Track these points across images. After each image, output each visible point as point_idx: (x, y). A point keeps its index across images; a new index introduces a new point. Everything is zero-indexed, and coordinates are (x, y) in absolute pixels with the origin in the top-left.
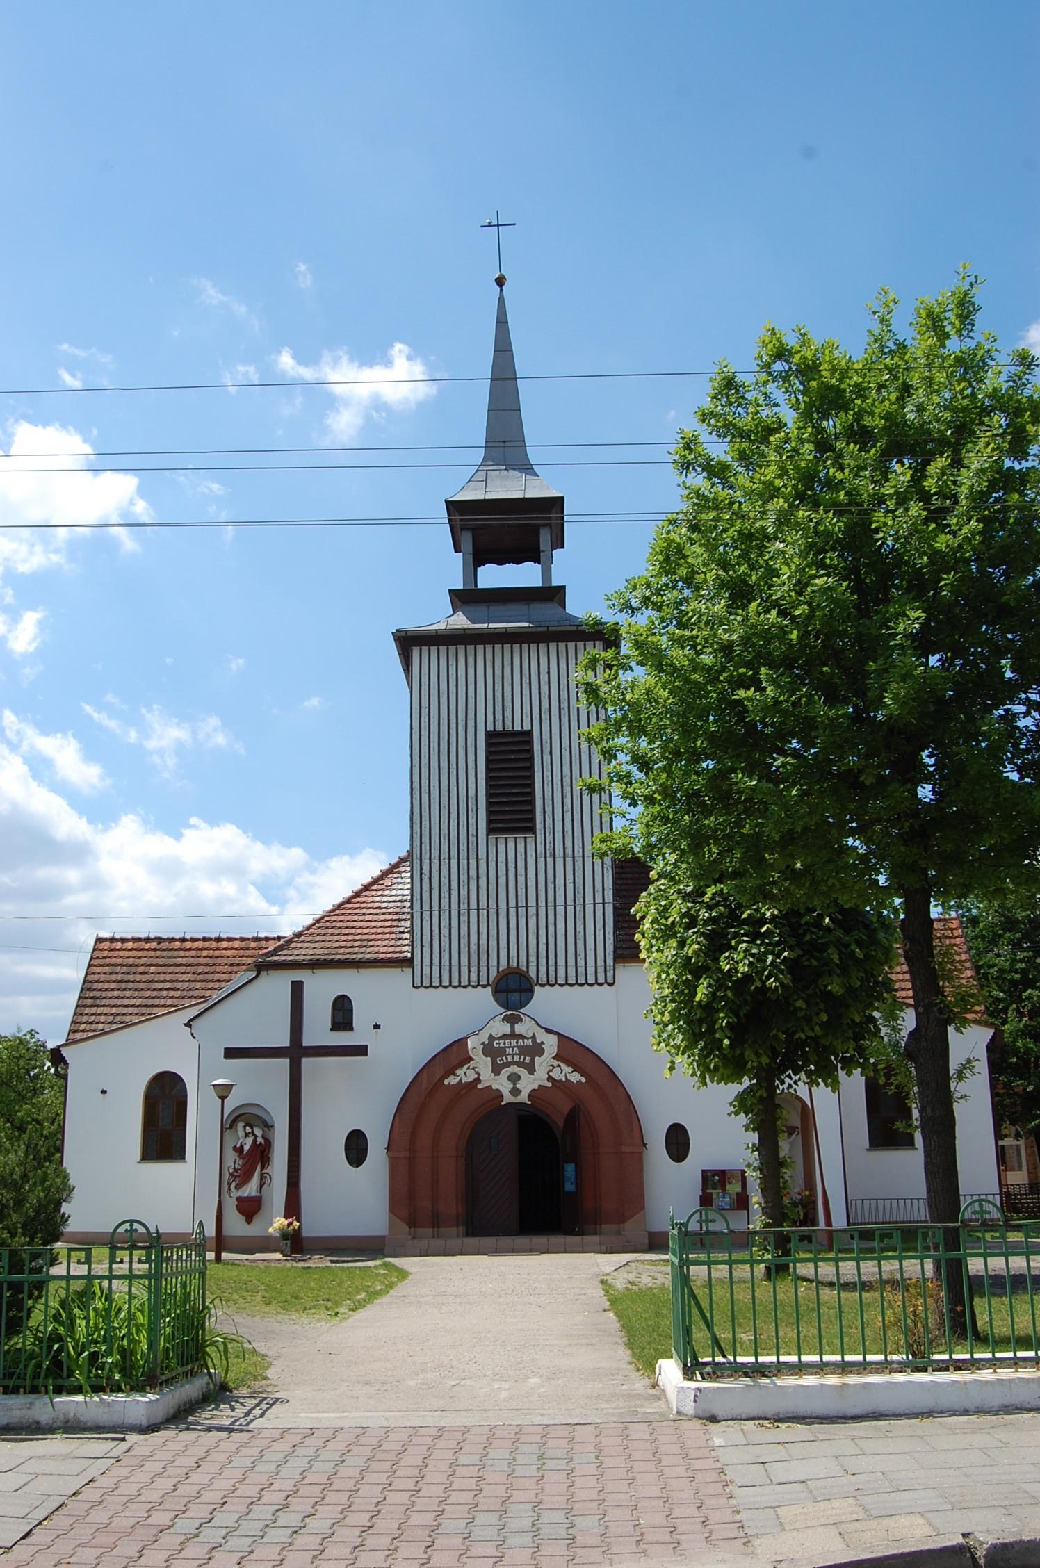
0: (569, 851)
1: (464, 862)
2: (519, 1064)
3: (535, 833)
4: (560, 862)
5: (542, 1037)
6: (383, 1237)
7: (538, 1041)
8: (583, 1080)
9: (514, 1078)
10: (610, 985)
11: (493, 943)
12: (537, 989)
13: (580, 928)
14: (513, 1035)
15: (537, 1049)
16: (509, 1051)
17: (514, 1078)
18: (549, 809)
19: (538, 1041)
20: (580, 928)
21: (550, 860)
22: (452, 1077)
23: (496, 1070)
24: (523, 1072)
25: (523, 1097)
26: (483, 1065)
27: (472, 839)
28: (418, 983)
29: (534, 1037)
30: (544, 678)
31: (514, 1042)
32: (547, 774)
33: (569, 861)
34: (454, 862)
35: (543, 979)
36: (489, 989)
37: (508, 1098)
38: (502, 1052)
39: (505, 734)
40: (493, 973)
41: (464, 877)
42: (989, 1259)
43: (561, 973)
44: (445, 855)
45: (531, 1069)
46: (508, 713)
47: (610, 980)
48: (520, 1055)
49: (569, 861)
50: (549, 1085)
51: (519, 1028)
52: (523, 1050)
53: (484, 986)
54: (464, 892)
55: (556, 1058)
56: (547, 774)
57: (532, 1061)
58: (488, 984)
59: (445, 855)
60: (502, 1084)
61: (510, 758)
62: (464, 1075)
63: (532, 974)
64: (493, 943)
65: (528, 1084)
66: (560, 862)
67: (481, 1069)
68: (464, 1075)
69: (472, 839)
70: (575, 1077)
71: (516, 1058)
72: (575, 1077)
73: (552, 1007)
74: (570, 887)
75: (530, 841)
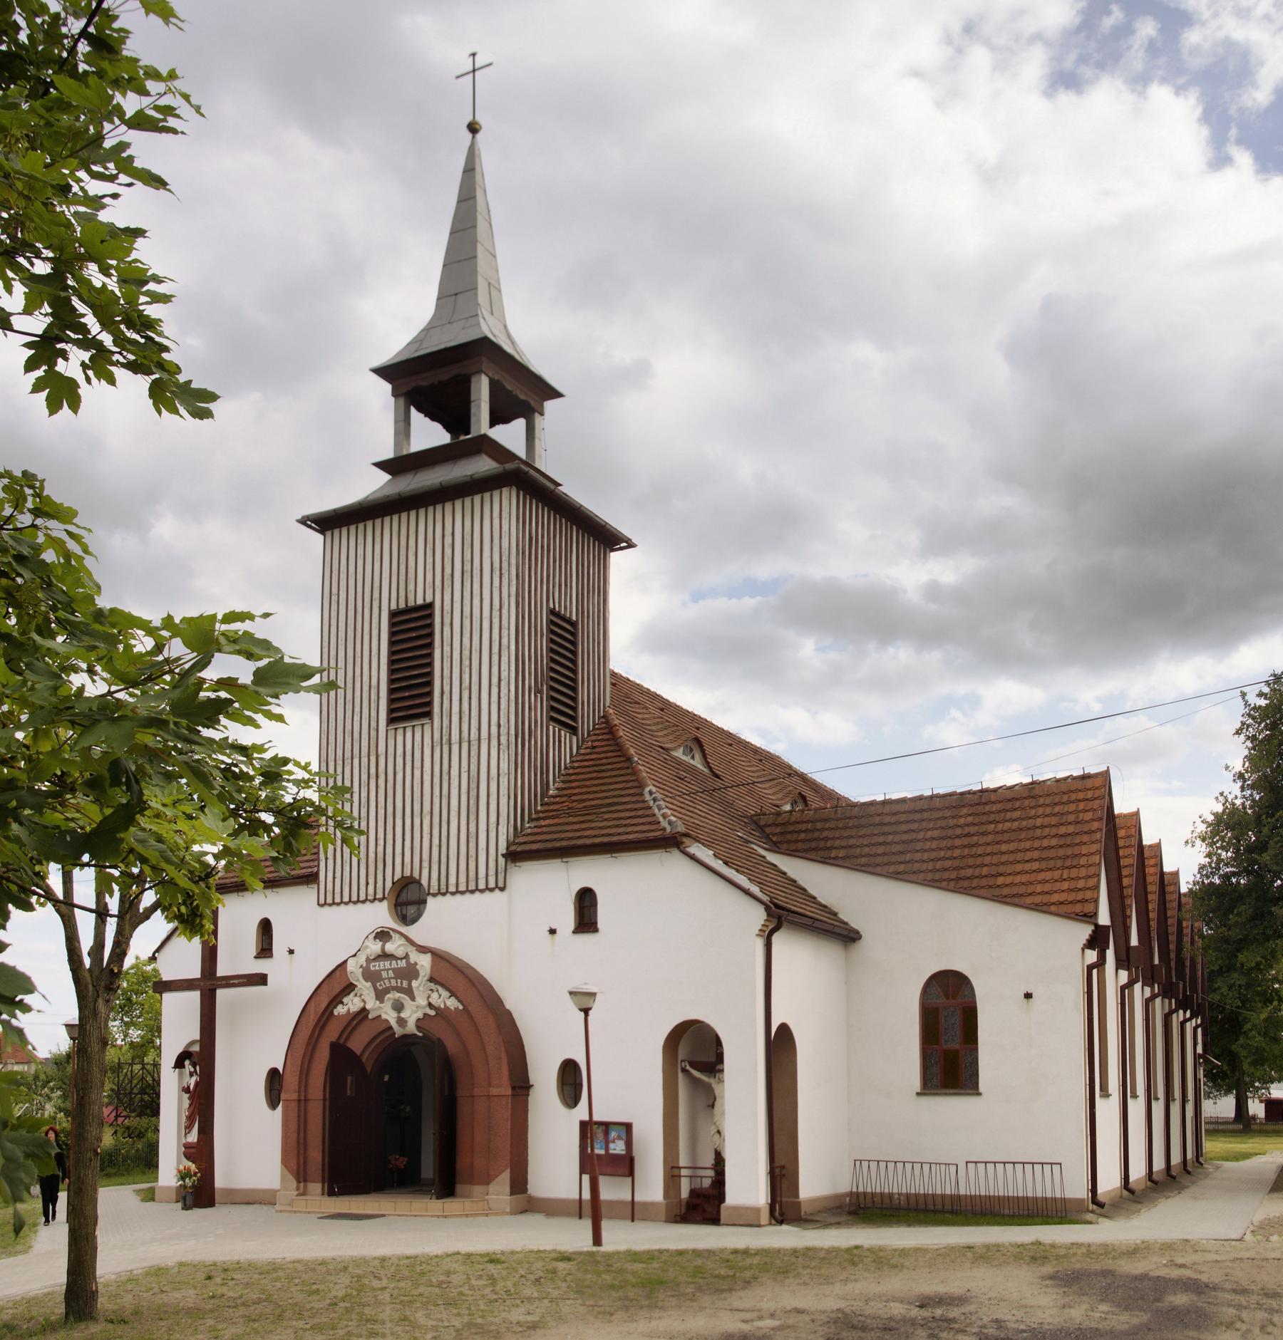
0: (465, 735)
1: (365, 760)
2: (399, 990)
3: (432, 719)
4: (455, 748)
5: (415, 957)
6: (276, 1191)
7: (412, 961)
8: (461, 1007)
9: (399, 1007)
10: (502, 889)
11: (389, 850)
12: (430, 900)
13: (473, 828)
14: (384, 956)
15: (410, 972)
16: (384, 974)
17: (399, 1007)
18: (447, 688)
19: (412, 961)
20: (473, 826)
21: (446, 748)
22: (340, 1006)
23: (380, 996)
24: (405, 999)
25: (411, 1028)
26: (365, 987)
27: (373, 733)
28: (322, 901)
29: (407, 957)
30: (448, 540)
31: (387, 964)
32: (447, 648)
33: (465, 746)
34: (356, 761)
35: (434, 889)
36: (385, 903)
37: (399, 1031)
38: (378, 973)
39: (408, 610)
40: (389, 884)
41: (364, 777)
42: (195, 996)
43: (452, 880)
44: (348, 754)
45: (410, 992)
46: (411, 586)
47: (501, 884)
48: (396, 978)
49: (465, 746)
50: (432, 1013)
51: (390, 947)
52: (399, 974)
53: (381, 900)
54: (364, 794)
55: (431, 980)
56: (447, 648)
57: (410, 984)
58: (384, 898)
59: (348, 754)
60: (390, 1016)
61: (412, 632)
62: (351, 1004)
63: (424, 882)
64: (389, 850)
65: (412, 1014)
66: (455, 748)
67: (362, 998)
68: (351, 1004)
69: (373, 733)
70: (452, 1003)
71: (393, 983)
72: (452, 1003)
73: (448, 924)
74: (465, 776)
75: (427, 728)
